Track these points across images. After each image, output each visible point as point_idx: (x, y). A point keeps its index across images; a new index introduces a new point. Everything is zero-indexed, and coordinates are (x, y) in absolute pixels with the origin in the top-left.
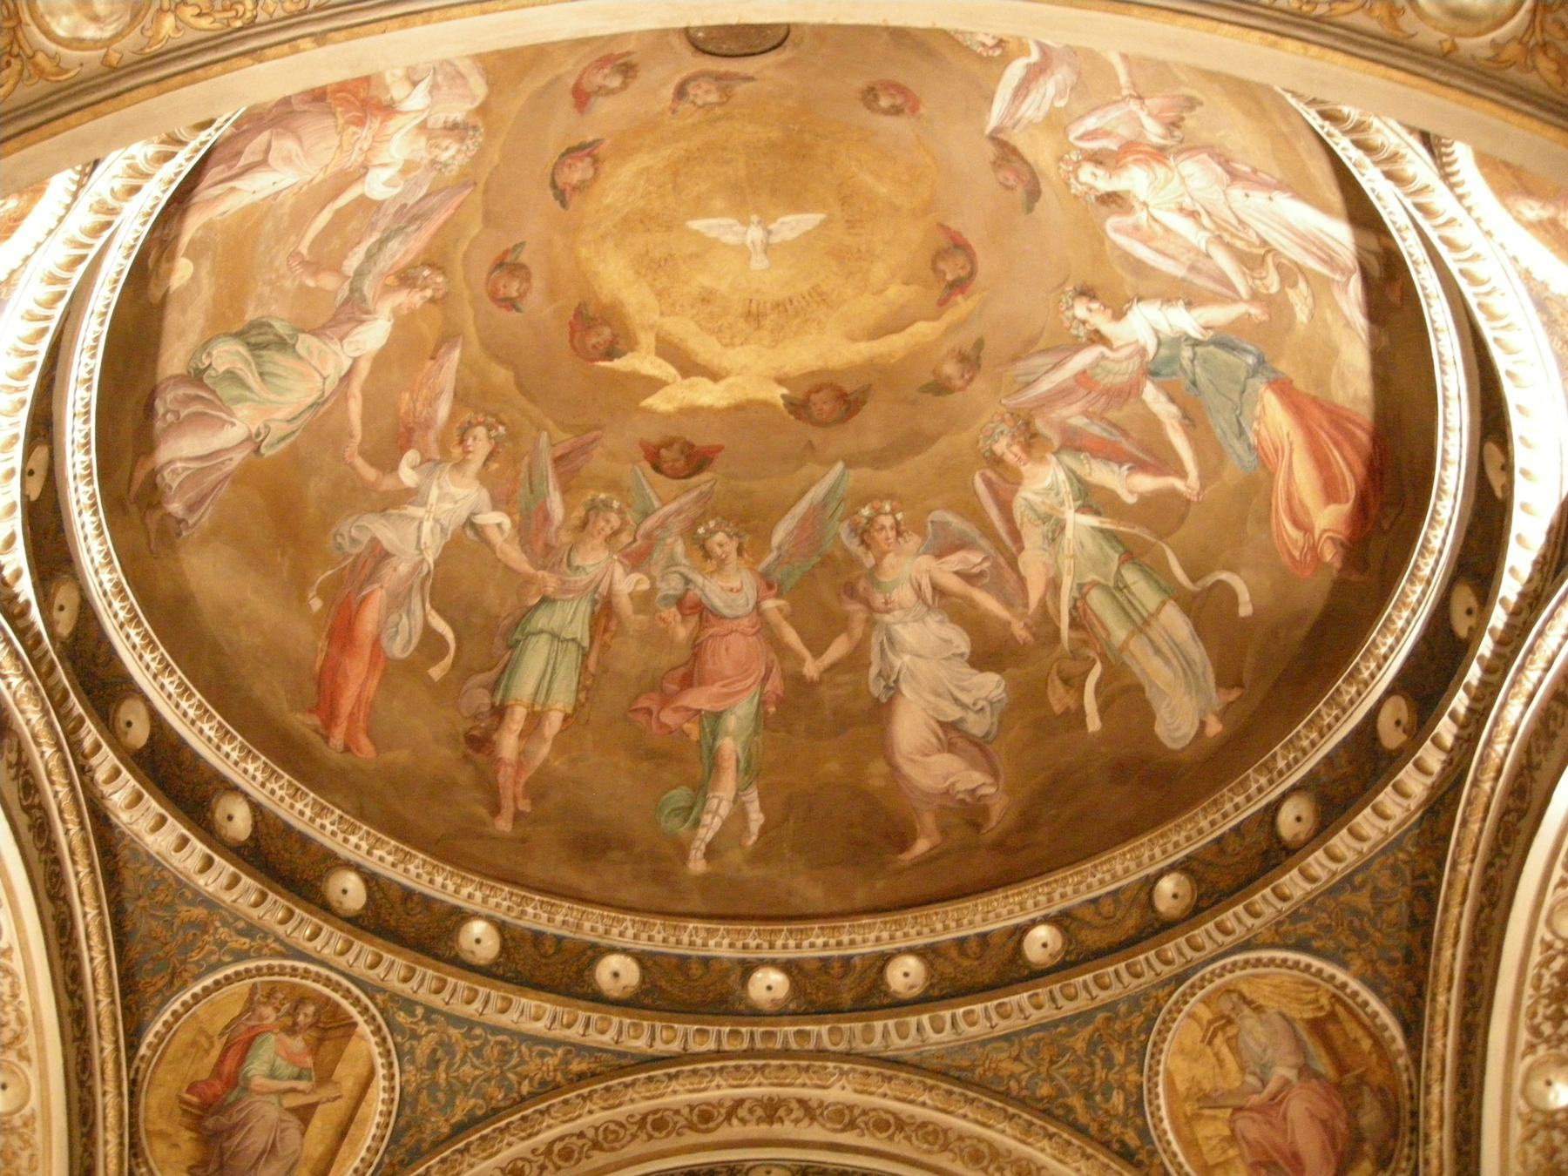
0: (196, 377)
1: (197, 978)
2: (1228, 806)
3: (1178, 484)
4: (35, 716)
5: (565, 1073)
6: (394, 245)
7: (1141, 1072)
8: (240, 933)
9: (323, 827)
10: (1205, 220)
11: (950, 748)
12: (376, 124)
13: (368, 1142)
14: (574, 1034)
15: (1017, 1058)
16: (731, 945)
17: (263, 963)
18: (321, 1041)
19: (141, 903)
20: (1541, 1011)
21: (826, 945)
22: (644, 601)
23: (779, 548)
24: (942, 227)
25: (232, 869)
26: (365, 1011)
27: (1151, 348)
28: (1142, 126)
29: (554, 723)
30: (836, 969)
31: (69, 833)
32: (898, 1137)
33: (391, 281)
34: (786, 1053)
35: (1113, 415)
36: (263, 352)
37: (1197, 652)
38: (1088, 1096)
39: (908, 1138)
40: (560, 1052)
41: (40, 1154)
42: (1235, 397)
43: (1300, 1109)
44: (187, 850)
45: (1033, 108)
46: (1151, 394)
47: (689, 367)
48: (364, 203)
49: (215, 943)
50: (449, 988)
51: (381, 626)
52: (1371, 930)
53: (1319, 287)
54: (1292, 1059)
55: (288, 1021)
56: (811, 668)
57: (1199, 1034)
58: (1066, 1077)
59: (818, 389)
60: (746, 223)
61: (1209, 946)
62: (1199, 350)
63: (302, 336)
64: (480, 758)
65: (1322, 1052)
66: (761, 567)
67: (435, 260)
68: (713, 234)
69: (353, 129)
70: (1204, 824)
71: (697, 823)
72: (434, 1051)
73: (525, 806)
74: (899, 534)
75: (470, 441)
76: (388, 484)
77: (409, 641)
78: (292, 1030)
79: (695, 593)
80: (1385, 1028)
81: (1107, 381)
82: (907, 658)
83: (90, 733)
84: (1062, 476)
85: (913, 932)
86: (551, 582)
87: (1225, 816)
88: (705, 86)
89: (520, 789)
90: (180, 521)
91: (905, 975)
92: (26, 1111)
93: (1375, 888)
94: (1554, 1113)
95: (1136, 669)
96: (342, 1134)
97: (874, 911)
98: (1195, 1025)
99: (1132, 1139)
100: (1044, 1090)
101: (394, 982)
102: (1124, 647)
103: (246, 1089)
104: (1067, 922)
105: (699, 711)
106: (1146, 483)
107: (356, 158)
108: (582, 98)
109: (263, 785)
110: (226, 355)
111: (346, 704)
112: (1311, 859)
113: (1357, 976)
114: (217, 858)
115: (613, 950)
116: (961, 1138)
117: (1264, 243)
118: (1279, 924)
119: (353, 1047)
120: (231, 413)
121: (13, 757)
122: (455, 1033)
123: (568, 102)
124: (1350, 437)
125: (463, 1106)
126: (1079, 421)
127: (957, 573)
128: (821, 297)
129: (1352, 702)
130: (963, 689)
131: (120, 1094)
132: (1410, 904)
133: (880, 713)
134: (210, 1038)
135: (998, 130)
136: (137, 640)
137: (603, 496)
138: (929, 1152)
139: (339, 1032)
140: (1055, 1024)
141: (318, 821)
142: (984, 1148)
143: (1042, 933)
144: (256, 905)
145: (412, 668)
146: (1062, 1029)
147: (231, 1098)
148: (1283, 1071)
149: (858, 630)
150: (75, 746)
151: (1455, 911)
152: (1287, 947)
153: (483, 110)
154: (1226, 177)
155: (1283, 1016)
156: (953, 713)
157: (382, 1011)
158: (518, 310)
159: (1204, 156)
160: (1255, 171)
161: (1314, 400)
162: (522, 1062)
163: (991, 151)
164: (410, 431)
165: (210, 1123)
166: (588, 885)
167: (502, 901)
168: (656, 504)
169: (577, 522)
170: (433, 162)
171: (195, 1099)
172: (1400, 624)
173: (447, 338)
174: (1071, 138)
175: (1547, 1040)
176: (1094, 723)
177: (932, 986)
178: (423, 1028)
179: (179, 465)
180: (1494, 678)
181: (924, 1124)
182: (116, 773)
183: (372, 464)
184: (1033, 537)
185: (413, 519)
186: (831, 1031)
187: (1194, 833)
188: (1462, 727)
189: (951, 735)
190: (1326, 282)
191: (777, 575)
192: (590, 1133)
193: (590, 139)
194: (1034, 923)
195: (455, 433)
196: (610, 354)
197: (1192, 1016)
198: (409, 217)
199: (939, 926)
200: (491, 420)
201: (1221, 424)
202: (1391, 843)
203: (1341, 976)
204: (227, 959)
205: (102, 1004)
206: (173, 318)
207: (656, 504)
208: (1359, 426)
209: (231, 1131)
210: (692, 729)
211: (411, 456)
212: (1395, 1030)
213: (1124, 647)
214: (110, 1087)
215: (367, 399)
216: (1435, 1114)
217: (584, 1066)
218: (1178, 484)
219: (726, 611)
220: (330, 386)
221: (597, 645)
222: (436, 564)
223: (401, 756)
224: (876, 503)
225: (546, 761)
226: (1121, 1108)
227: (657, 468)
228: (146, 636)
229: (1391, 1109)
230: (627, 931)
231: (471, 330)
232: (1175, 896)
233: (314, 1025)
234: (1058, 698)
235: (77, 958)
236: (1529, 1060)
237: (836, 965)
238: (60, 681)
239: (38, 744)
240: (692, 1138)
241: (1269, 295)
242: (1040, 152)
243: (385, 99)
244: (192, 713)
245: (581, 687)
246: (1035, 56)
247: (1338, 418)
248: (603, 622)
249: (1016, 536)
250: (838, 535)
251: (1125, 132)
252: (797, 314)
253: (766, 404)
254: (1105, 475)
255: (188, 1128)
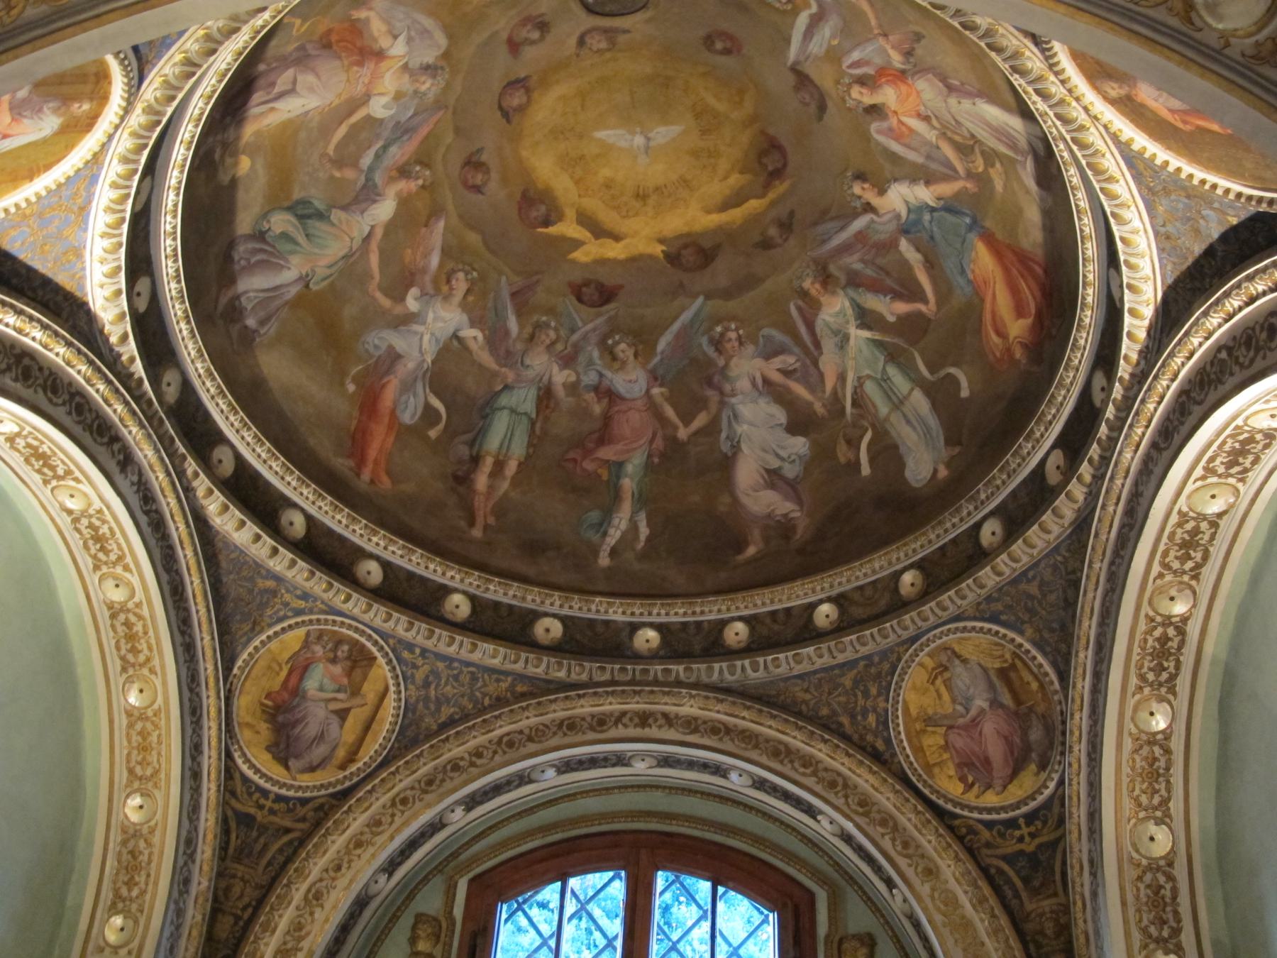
0: (260, 236)
1: (270, 626)
2: (948, 525)
3: (922, 307)
4: (150, 453)
5: (513, 693)
6: (393, 149)
7: (887, 700)
8: (299, 597)
9: (354, 531)
10: (935, 122)
11: (771, 486)
12: (372, 65)
13: (384, 734)
14: (519, 667)
15: (807, 691)
16: (624, 613)
17: (314, 617)
18: (352, 668)
19: (232, 577)
20: (1146, 664)
21: (685, 614)
22: (573, 388)
23: (662, 353)
24: (763, 132)
25: (291, 556)
26: (381, 649)
27: (904, 214)
28: (889, 56)
29: (511, 468)
30: (692, 630)
31: (179, 529)
32: (726, 739)
33: (394, 173)
34: (656, 682)
35: (881, 261)
36: (309, 221)
37: (933, 422)
38: (853, 716)
39: (732, 740)
40: (510, 679)
41: (163, 732)
42: (958, 246)
43: (991, 728)
44: (260, 543)
45: (817, 46)
46: (904, 245)
47: (600, 232)
48: (369, 120)
49: (282, 603)
50: (436, 636)
51: (396, 403)
52: (1039, 609)
53: (1009, 164)
54: (986, 695)
55: (331, 655)
56: (683, 433)
57: (926, 677)
58: (839, 703)
59: (686, 246)
60: (633, 133)
61: (932, 619)
62: (935, 214)
63: (334, 211)
64: (461, 489)
65: (1006, 690)
66: (651, 366)
67: (423, 159)
68: (611, 141)
69: (355, 68)
70: (932, 536)
71: (605, 534)
72: (427, 677)
73: (491, 520)
74: (741, 344)
75: (454, 282)
76: (398, 310)
77: (414, 414)
78: (334, 661)
79: (606, 383)
80: (1046, 674)
81: (876, 238)
82: (745, 427)
83: (191, 465)
84: (847, 304)
85: (742, 606)
86: (510, 376)
87: (946, 531)
88: (597, 38)
89: (488, 509)
90: (255, 331)
91: (737, 633)
92: (156, 706)
93: (1042, 579)
94: (1170, 617)
95: (893, 433)
96: (367, 727)
97: (718, 592)
98: (923, 670)
99: (880, 745)
100: (825, 711)
101: (400, 631)
102: (887, 419)
103: (304, 697)
104: (842, 601)
105: (608, 461)
106: (902, 307)
107: (360, 89)
108: (514, 46)
109: (313, 503)
110: (280, 222)
111: (372, 453)
112: (998, 560)
113: (1028, 640)
114: (281, 549)
115: (546, 615)
116: (767, 741)
117: (973, 136)
118: (979, 604)
119: (374, 673)
120: (287, 261)
121: (135, 479)
122: (441, 665)
123: (504, 49)
124: (1030, 270)
125: (446, 712)
126: (858, 266)
127: (778, 370)
128: (685, 182)
129: (1029, 453)
130: (783, 448)
131: (219, 698)
132: (1065, 592)
133: (727, 464)
134: (280, 665)
135: (796, 63)
136: (224, 407)
137: (544, 318)
138: (746, 749)
139: (365, 663)
140: (832, 668)
141: (351, 527)
142: (782, 748)
143: (825, 608)
144: (307, 580)
145: (416, 431)
146: (836, 672)
147: (295, 703)
148: (980, 703)
149: (713, 407)
150: (181, 474)
151: (1090, 595)
152: (983, 620)
153: (446, 55)
154: (945, 89)
155: (980, 665)
156: (775, 463)
157: (393, 650)
158: (482, 194)
159: (930, 76)
160: (963, 84)
161: (1009, 246)
162: (485, 685)
163: (791, 79)
164: (412, 274)
165: (280, 718)
166: (531, 571)
167: (472, 581)
168: (580, 324)
169: (526, 336)
170: (416, 92)
171: (269, 703)
172: (1060, 399)
173: (436, 211)
174: (844, 67)
175: (1151, 685)
176: (866, 470)
177: (753, 642)
178: (420, 662)
179: (252, 294)
180: (1115, 434)
181: (743, 731)
182: (210, 492)
183: (386, 295)
184: (828, 345)
185: (416, 333)
186: (686, 669)
187: (925, 542)
188: (1096, 469)
189: (773, 478)
190: (1013, 161)
191: (660, 372)
192: (527, 731)
193: (523, 75)
194: (821, 602)
195: (444, 277)
196: (547, 223)
197: (921, 665)
198: (402, 130)
199: (759, 602)
200: (467, 268)
201: (950, 265)
202: (1051, 551)
203: (1019, 640)
204: (290, 614)
205: (206, 639)
206: (242, 196)
207: (580, 324)
208: (1037, 263)
209: (297, 722)
210: (605, 475)
211: (414, 292)
212: (1053, 676)
213: (887, 419)
214: (212, 693)
215: (382, 252)
216: (1077, 733)
217: (525, 689)
218: (922, 307)
219: (628, 396)
220: (357, 244)
221: (541, 417)
222: (433, 362)
223: (409, 487)
224: (725, 324)
225: (506, 494)
226: (874, 725)
227: (580, 300)
228: (230, 404)
229: (1049, 729)
230: (554, 602)
231: (450, 207)
232: (912, 585)
233: (348, 658)
234: (843, 453)
235: (187, 610)
236: (1138, 697)
237: (692, 627)
238: (167, 431)
239: (154, 471)
240: (591, 736)
241: (978, 174)
242: (824, 77)
243: (376, 47)
244: (264, 455)
245: (530, 445)
246: (814, 9)
247: (1023, 258)
248: (545, 402)
249: (817, 344)
250: (700, 345)
251: (878, 61)
252: (670, 196)
253: (651, 257)
254: (876, 303)
255: (265, 721)
